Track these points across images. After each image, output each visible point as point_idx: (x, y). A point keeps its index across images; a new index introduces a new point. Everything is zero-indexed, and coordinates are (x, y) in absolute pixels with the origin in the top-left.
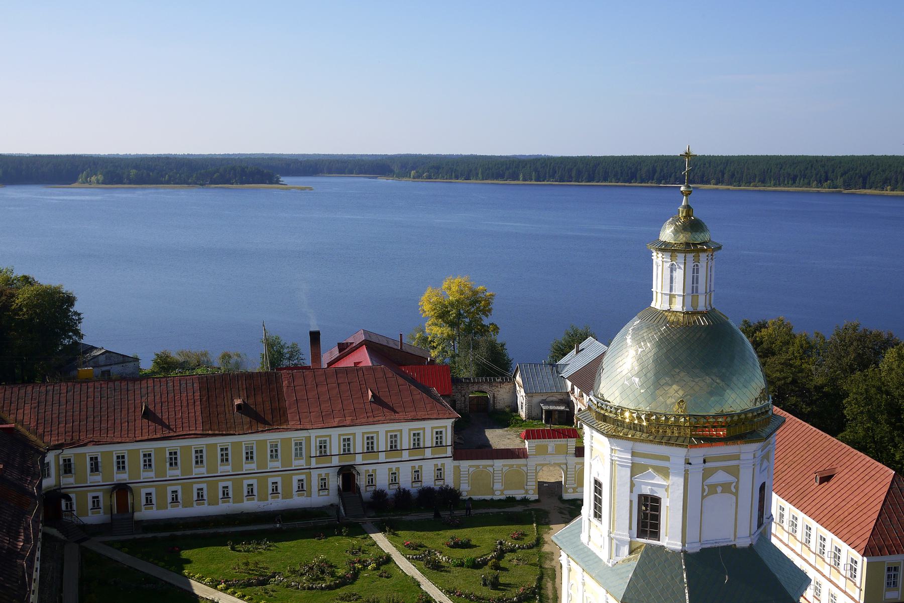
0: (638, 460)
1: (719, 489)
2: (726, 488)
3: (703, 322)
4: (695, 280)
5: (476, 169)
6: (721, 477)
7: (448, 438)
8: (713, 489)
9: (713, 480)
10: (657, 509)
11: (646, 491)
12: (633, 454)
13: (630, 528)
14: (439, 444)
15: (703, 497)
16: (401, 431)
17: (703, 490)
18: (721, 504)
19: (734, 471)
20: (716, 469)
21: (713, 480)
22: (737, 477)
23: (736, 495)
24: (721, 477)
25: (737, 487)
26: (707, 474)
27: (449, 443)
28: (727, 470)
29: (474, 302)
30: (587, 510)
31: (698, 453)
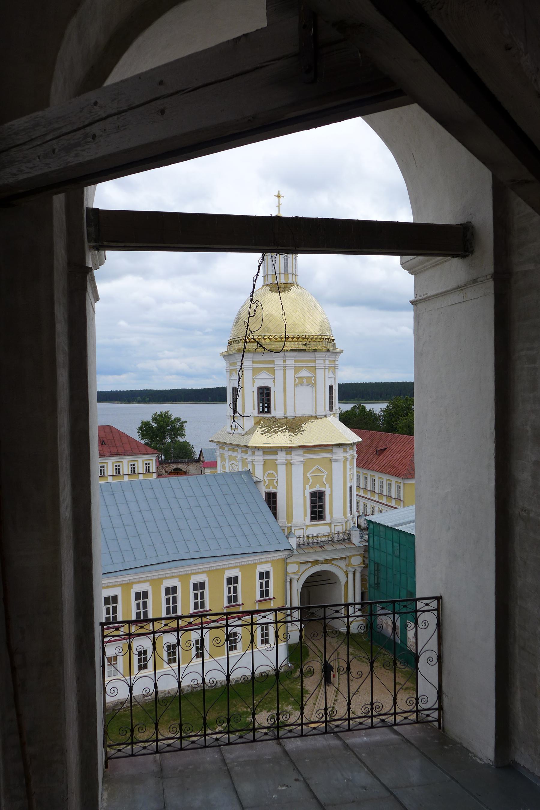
0: (256, 366)
6: (304, 373)
7: (153, 468)
10: (268, 394)
11: (261, 385)
12: (253, 362)
14: (148, 471)
15: (295, 385)
17: (295, 380)
18: (305, 392)
20: (261, 369)
26: (297, 370)
29: (173, 429)
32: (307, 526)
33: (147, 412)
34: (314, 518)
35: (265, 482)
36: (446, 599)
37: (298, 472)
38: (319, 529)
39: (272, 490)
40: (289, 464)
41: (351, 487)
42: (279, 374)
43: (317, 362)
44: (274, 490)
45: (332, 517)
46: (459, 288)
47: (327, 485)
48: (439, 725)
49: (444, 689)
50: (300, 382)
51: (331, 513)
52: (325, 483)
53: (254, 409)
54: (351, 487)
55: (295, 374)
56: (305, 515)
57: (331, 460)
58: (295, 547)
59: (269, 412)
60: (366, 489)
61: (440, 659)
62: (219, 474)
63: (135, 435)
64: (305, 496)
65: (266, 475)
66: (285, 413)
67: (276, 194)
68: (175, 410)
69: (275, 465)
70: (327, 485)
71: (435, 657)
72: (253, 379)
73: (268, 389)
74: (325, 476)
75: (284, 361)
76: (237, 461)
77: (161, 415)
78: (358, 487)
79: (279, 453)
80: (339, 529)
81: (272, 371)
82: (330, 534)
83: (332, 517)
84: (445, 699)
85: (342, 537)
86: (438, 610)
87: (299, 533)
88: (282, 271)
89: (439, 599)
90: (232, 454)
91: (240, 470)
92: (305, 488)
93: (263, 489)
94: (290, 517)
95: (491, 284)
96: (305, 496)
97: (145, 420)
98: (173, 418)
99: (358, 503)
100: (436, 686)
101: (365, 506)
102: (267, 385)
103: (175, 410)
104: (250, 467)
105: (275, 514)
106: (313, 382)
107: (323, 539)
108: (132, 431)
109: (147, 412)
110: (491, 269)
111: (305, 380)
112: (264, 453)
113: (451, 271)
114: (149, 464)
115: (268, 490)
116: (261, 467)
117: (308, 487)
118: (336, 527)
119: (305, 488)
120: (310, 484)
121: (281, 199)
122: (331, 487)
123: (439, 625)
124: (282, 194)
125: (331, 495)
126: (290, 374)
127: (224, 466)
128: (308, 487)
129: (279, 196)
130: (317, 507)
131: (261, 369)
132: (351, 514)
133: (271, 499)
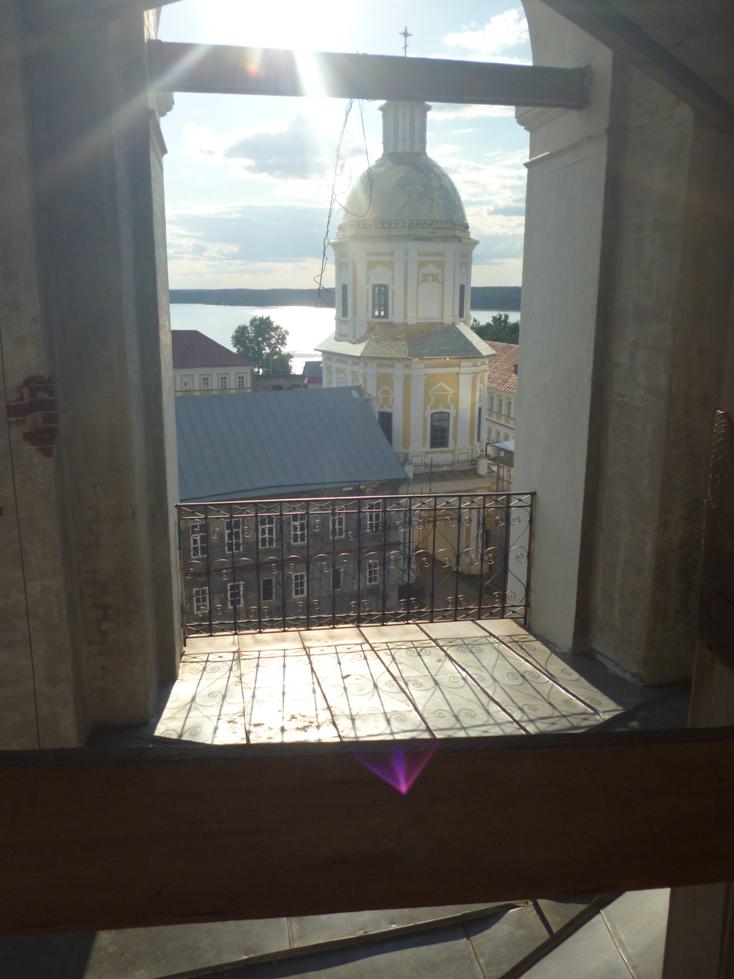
1: (430, 278)
2: (435, 278)
3: (355, 394)
4: (396, 129)
5: (403, 220)
6: (431, 269)
8: (425, 278)
9: (425, 270)
10: (386, 295)
13: (393, 293)
15: (418, 284)
16: (228, 374)
17: (418, 278)
19: (441, 265)
21: (425, 270)
22: (443, 269)
23: (442, 283)
24: (431, 269)
25: (443, 278)
26: (421, 265)
27: (249, 386)
31: (415, 247)
32: (427, 453)
33: (246, 315)
34: (434, 444)
36: (539, 494)
38: (441, 457)
39: (386, 409)
41: (480, 409)
46: (574, 147)
48: (525, 621)
49: (532, 585)
51: (455, 439)
56: (424, 441)
57: (458, 374)
58: (411, 476)
59: (386, 316)
60: (499, 413)
61: (529, 555)
62: (325, 389)
63: (228, 344)
64: (425, 419)
66: (405, 317)
67: (403, 30)
68: (278, 315)
71: (526, 554)
73: (386, 287)
76: (345, 374)
77: (261, 319)
78: (491, 410)
79: (397, 365)
80: (463, 457)
82: (453, 464)
84: (533, 596)
85: (467, 466)
86: (531, 506)
87: (416, 460)
89: (533, 494)
90: (341, 365)
91: (350, 385)
93: (377, 409)
94: (406, 444)
95: (604, 141)
98: (275, 325)
99: (490, 430)
100: (525, 583)
101: (490, 430)
103: (278, 315)
104: (361, 382)
105: (389, 438)
107: (445, 468)
108: (225, 340)
109: (246, 315)
110: (605, 124)
112: (379, 365)
113: (568, 124)
114: (243, 377)
115: (382, 410)
117: (429, 407)
119: (425, 409)
123: (531, 522)
124: (409, 31)
127: (331, 381)
128: (429, 407)
129: (406, 34)
132: (479, 440)
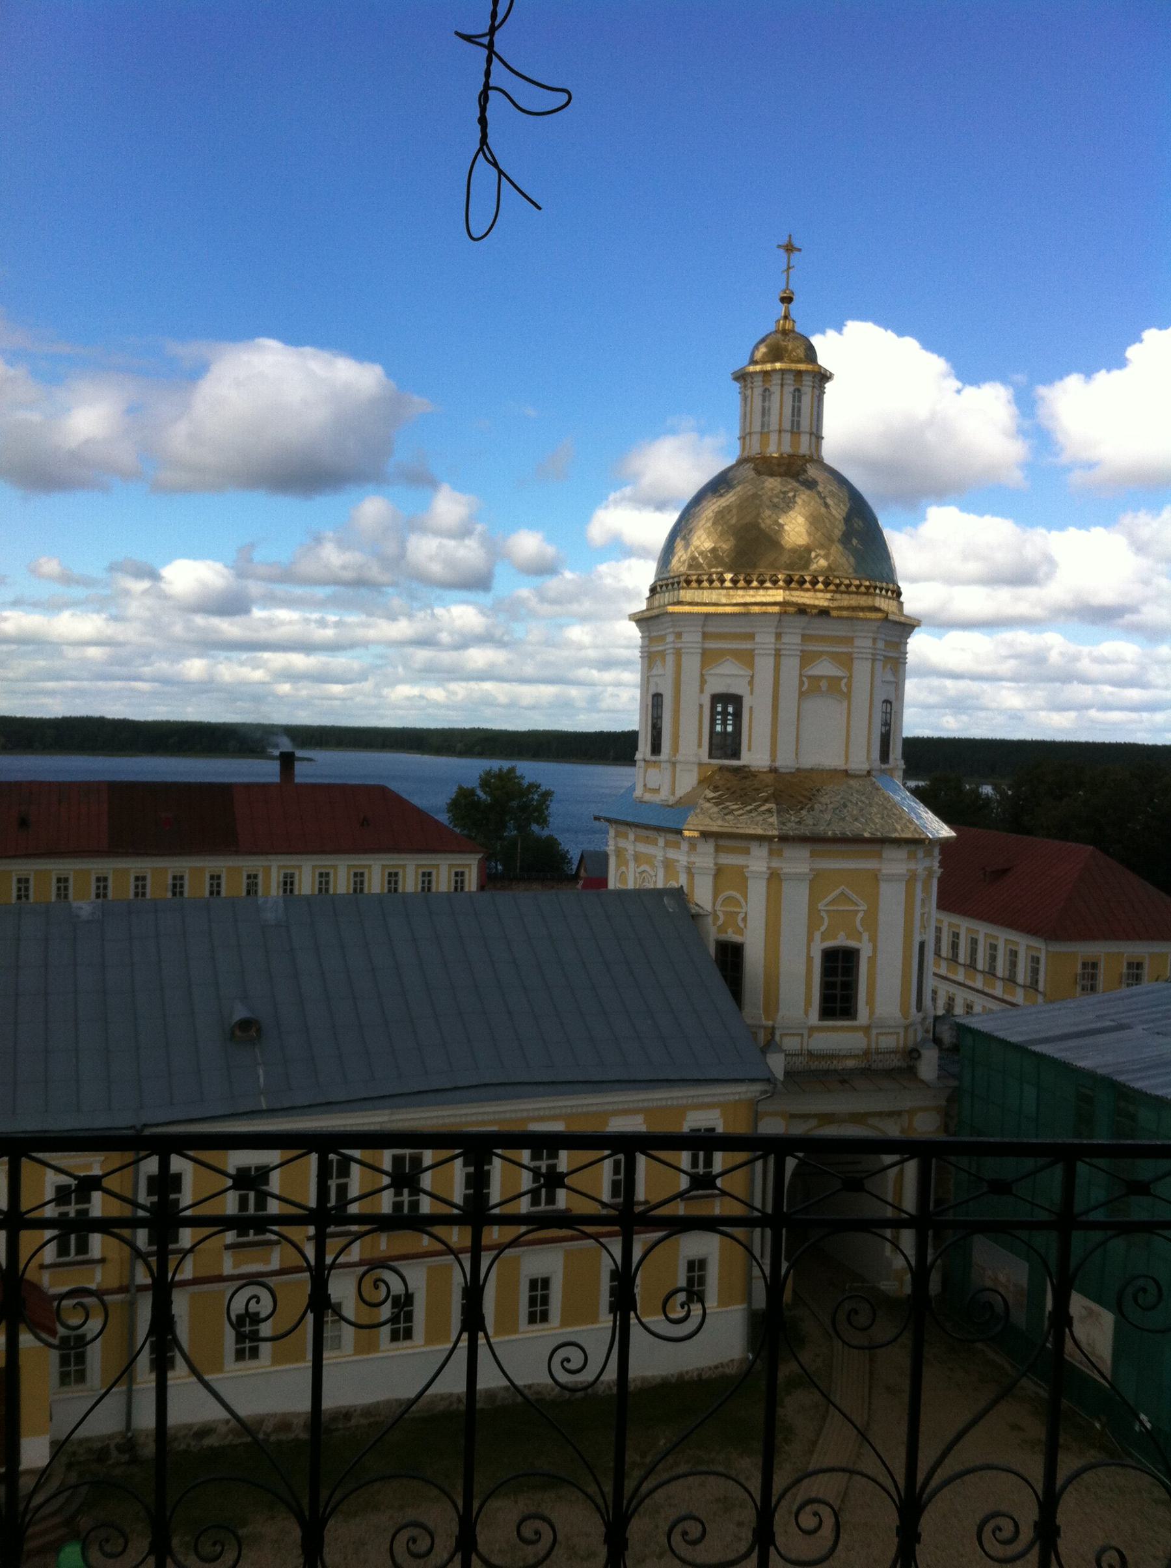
0: (712, 645)
6: (825, 668)
11: (720, 689)
12: (705, 636)
17: (801, 683)
23: (848, 696)
26: (807, 658)
28: (836, 657)
30: (644, 749)
35: (716, 917)
37: (796, 897)
38: (840, 1039)
40: (774, 878)
41: (922, 945)
42: (764, 665)
43: (858, 642)
44: (737, 938)
45: (872, 1013)
47: (865, 936)
50: (811, 688)
51: (871, 1001)
52: (861, 929)
53: (700, 746)
54: (922, 945)
55: (802, 667)
65: (720, 900)
69: (741, 878)
70: (865, 936)
72: (702, 676)
74: (860, 915)
75: (778, 636)
81: (747, 658)
83: (872, 1013)
88: (787, 425)
92: (810, 940)
93: (713, 934)
96: (810, 959)
97: (467, 785)
102: (733, 690)
106: (845, 689)
111: (824, 684)
115: (723, 937)
116: (709, 880)
117: (817, 936)
118: (882, 1038)
119: (810, 940)
120: (823, 928)
121: (796, 257)
122: (873, 940)
125: (872, 960)
126: (791, 665)
130: (839, 978)
131: (720, 654)
133: (730, 957)
